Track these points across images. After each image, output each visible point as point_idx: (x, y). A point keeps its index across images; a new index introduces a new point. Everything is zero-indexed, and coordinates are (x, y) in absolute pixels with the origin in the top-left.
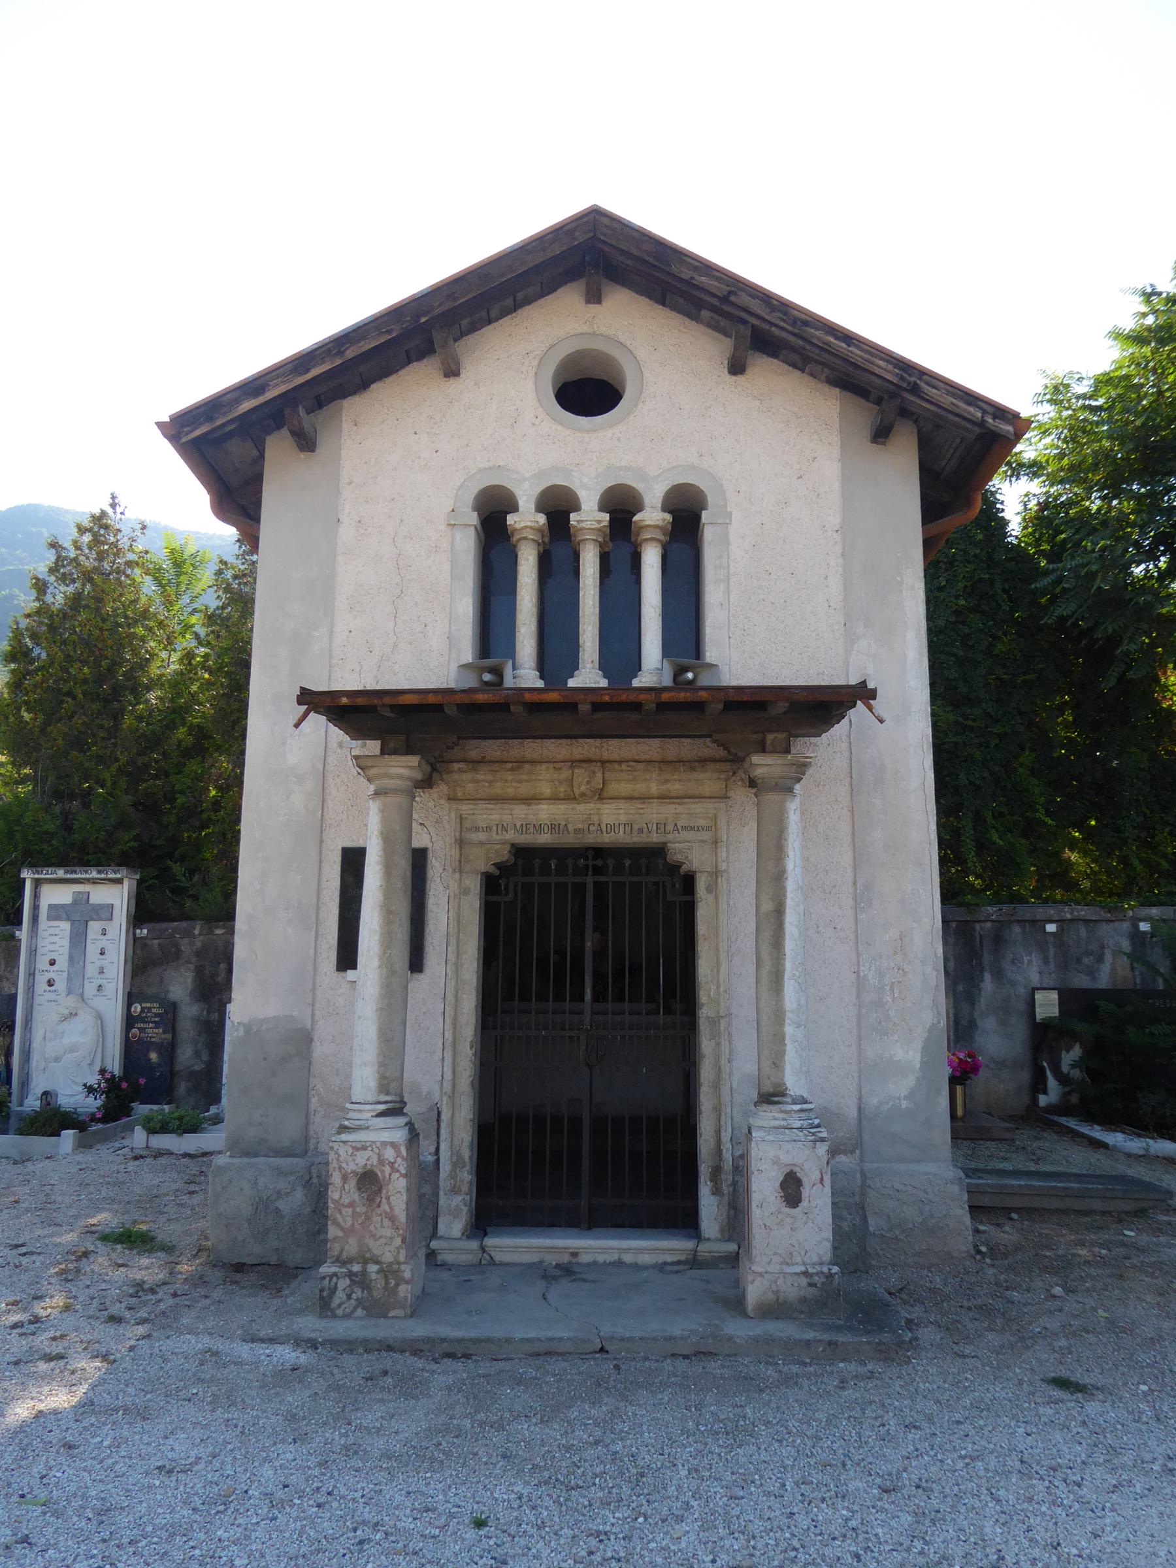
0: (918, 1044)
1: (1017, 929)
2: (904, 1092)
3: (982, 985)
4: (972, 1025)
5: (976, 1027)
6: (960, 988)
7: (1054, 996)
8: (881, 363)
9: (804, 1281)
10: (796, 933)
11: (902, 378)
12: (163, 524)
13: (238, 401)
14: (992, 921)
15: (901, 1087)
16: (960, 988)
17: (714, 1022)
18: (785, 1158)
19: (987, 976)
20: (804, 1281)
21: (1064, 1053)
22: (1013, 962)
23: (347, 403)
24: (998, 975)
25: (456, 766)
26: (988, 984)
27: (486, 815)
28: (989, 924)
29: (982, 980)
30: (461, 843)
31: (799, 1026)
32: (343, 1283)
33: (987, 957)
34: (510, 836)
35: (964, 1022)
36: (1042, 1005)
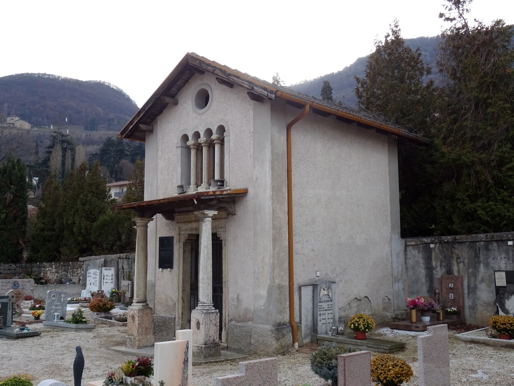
0: (266, 290)
1: (495, 244)
2: (263, 304)
3: (480, 270)
4: (476, 287)
5: (477, 288)
6: (470, 270)
7: (503, 274)
8: (245, 82)
9: (197, 348)
10: (203, 259)
11: (250, 86)
12: (426, 37)
13: (129, 127)
14: (483, 241)
15: (262, 302)
16: (470, 270)
17: (225, 282)
18: (197, 318)
19: (482, 265)
20: (197, 348)
21: (506, 300)
22: (493, 259)
23: (158, 117)
24: (487, 265)
25: (176, 214)
26: (482, 268)
27: (184, 227)
28: (483, 243)
29: (479, 267)
30: (179, 234)
31: (203, 283)
32: (128, 340)
33: (482, 258)
34: (188, 232)
35: (472, 286)
36: (498, 279)
